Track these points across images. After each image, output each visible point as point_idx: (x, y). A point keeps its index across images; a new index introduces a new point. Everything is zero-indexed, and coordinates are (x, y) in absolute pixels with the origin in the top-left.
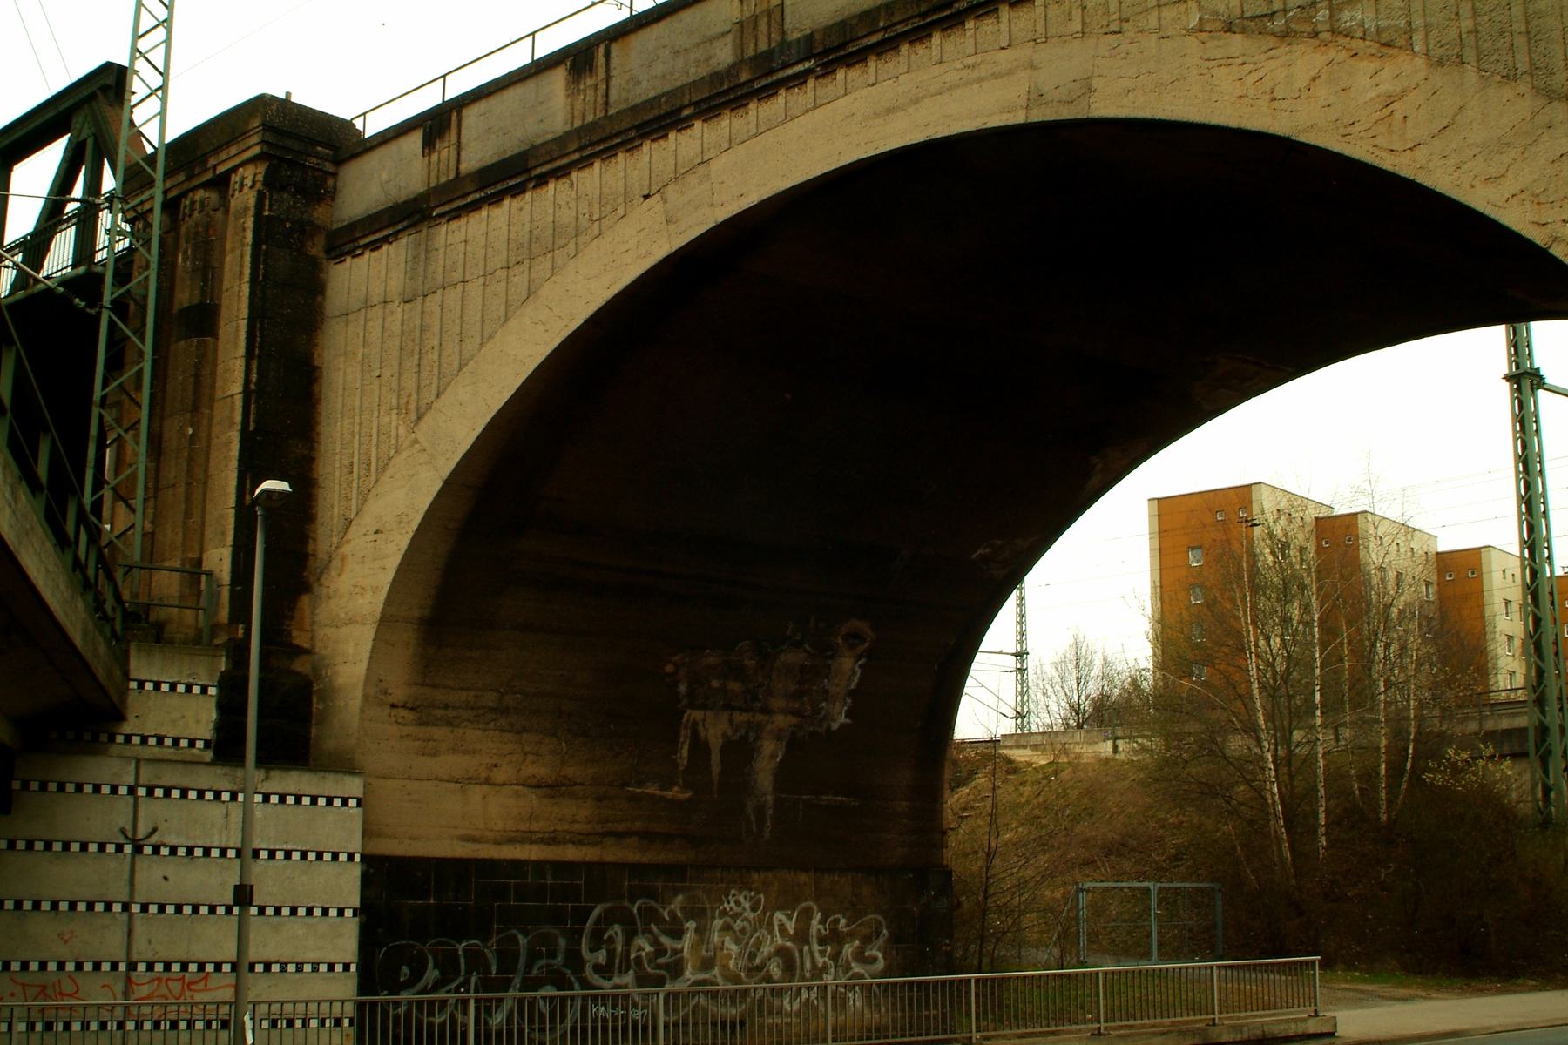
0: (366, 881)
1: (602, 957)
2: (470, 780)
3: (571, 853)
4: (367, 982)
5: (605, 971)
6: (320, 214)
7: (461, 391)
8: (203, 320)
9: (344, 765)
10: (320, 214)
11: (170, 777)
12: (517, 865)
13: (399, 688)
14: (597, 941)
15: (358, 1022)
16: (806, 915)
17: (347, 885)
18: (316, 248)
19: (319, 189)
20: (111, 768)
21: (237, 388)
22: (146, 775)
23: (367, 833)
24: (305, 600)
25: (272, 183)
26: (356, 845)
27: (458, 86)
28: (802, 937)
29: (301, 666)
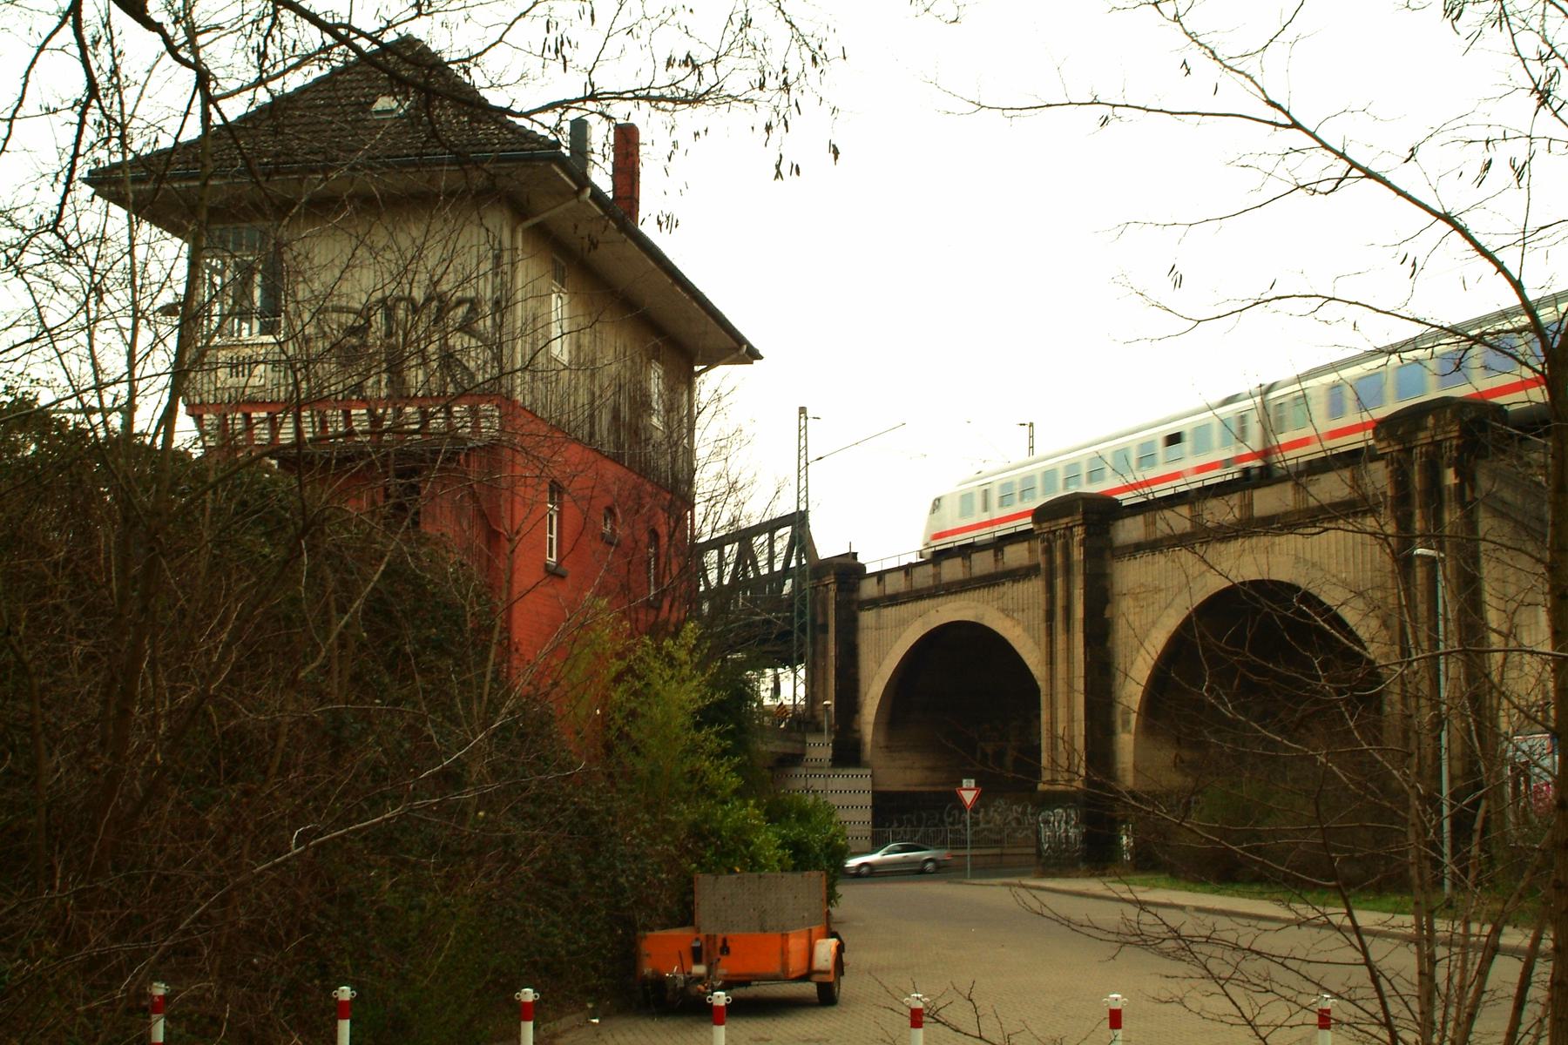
0: (873, 798)
1: (951, 819)
2: (906, 768)
3: (940, 788)
4: (875, 825)
5: (952, 824)
6: (855, 596)
7: (887, 661)
8: (824, 628)
9: (866, 766)
10: (855, 596)
11: (816, 771)
12: (922, 793)
13: (882, 741)
14: (949, 815)
15: (872, 838)
16: (1025, 808)
17: (867, 799)
18: (854, 607)
19: (855, 588)
20: (801, 770)
21: (833, 654)
22: (810, 771)
23: (873, 784)
24: (1109, 606)
25: (839, 590)
26: (870, 788)
27: (886, 567)
28: (1024, 813)
29: (857, 735)
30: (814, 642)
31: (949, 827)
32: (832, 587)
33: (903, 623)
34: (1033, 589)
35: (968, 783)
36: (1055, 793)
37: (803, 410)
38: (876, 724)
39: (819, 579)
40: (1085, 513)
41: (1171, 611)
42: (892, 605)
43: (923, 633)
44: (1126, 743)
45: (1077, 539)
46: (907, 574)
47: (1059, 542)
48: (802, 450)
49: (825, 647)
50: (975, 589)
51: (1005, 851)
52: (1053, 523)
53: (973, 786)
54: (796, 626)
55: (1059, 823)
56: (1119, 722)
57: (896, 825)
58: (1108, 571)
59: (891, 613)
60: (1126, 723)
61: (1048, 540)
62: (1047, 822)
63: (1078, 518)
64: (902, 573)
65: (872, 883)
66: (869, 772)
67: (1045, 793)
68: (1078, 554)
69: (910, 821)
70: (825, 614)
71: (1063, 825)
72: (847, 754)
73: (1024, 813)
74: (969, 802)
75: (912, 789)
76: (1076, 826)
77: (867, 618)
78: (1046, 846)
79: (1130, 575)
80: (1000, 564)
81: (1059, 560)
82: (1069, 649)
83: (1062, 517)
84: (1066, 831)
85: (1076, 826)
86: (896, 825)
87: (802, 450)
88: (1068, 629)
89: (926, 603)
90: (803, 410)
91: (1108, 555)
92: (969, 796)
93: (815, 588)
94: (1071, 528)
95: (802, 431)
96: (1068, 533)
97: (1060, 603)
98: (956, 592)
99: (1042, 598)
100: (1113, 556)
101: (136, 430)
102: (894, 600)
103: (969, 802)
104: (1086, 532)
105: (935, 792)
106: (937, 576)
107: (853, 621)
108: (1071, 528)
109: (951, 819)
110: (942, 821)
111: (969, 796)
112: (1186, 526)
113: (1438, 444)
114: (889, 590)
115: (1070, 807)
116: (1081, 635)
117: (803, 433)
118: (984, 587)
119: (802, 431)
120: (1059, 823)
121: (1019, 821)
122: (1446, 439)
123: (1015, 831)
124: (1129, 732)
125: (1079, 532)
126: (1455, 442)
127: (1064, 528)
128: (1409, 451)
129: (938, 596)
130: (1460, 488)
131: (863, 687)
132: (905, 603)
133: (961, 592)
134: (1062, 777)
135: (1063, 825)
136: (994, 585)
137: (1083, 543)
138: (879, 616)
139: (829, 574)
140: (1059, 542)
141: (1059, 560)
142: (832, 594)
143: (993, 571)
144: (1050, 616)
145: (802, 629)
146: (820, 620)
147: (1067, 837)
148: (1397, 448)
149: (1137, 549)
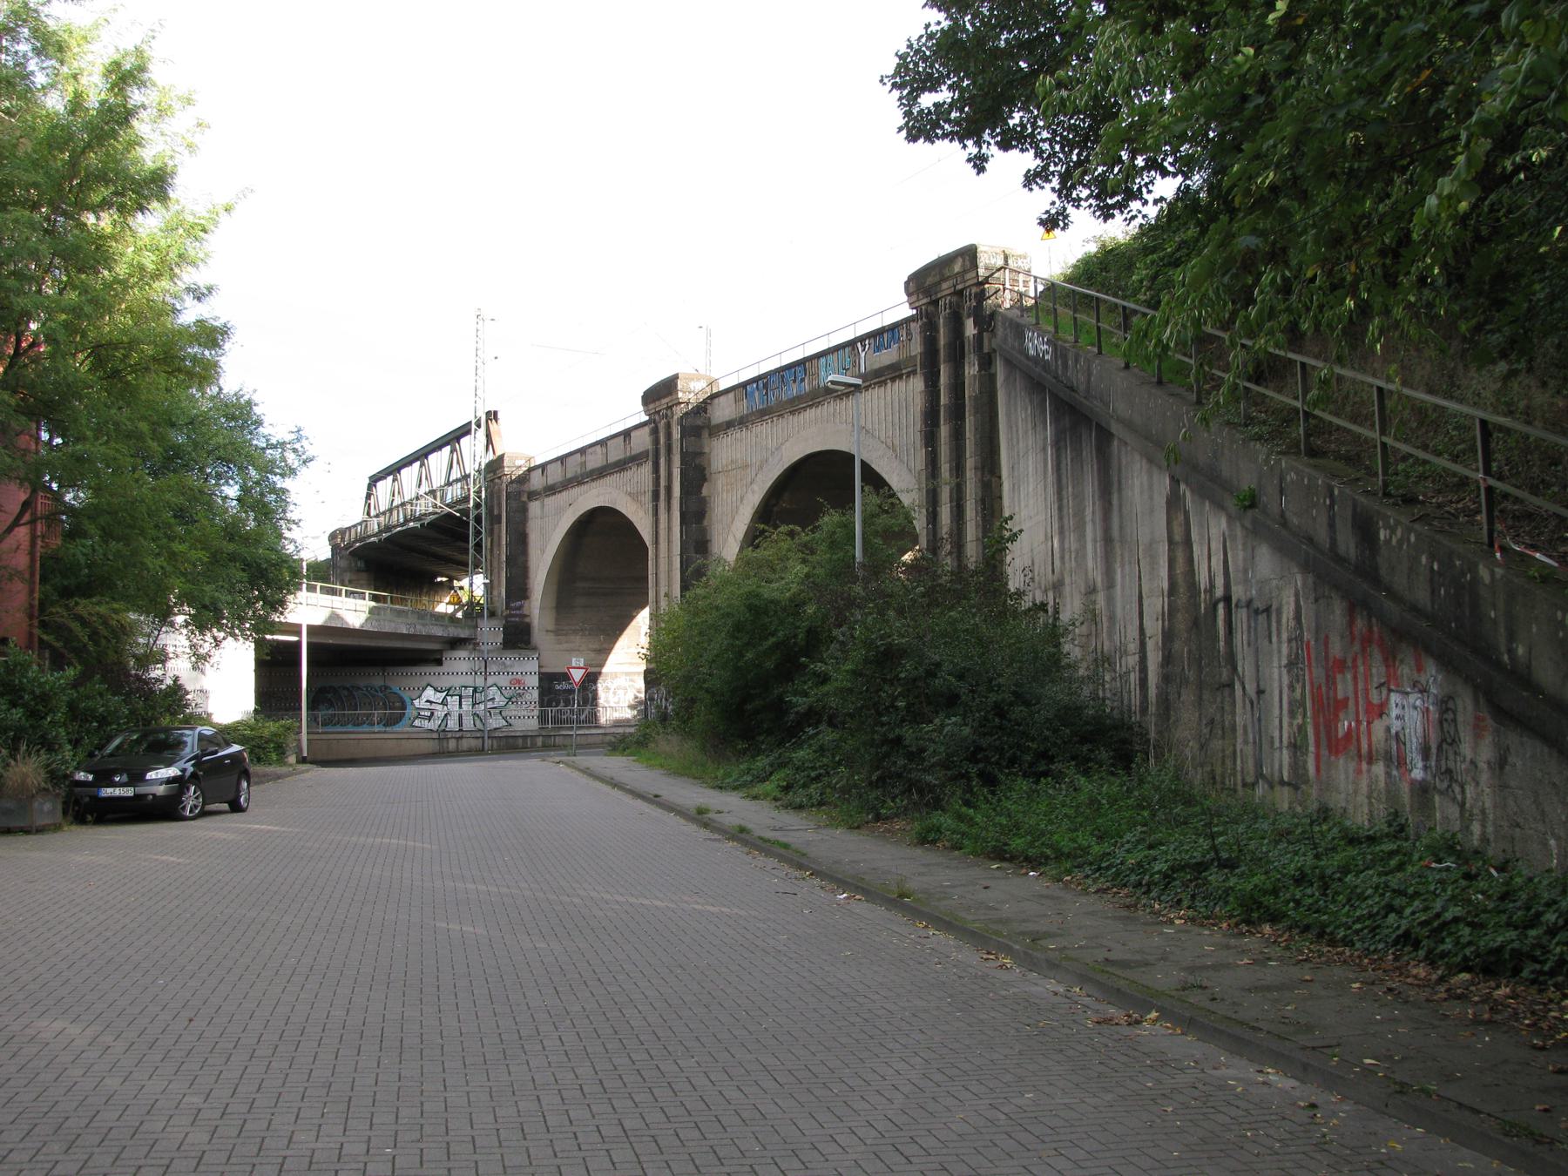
0: (540, 680)
4: (541, 705)
13: (551, 626)
18: (524, 498)
30: (491, 533)
33: (560, 511)
34: (644, 473)
41: (755, 487)
50: (610, 474)
58: (706, 450)
59: (551, 501)
65: (460, 762)
74: (577, 680)
77: (534, 508)
88: (669, 509)
89: (575, 491)
91: (705, 434)
97: (663, 483)
100: (710, 435)
101: (647, 418)
102: (551, 490)
103: (577, 680)
106: (584, 464)
113: (960, 293)
122: (965, 288)
128: (935, 303)
130: (979, 338)
136: (623, 470)
138: (543, 506)
144: (656, 496)
145: (478, 519)
146: (496, 512)
148: (925, 301)
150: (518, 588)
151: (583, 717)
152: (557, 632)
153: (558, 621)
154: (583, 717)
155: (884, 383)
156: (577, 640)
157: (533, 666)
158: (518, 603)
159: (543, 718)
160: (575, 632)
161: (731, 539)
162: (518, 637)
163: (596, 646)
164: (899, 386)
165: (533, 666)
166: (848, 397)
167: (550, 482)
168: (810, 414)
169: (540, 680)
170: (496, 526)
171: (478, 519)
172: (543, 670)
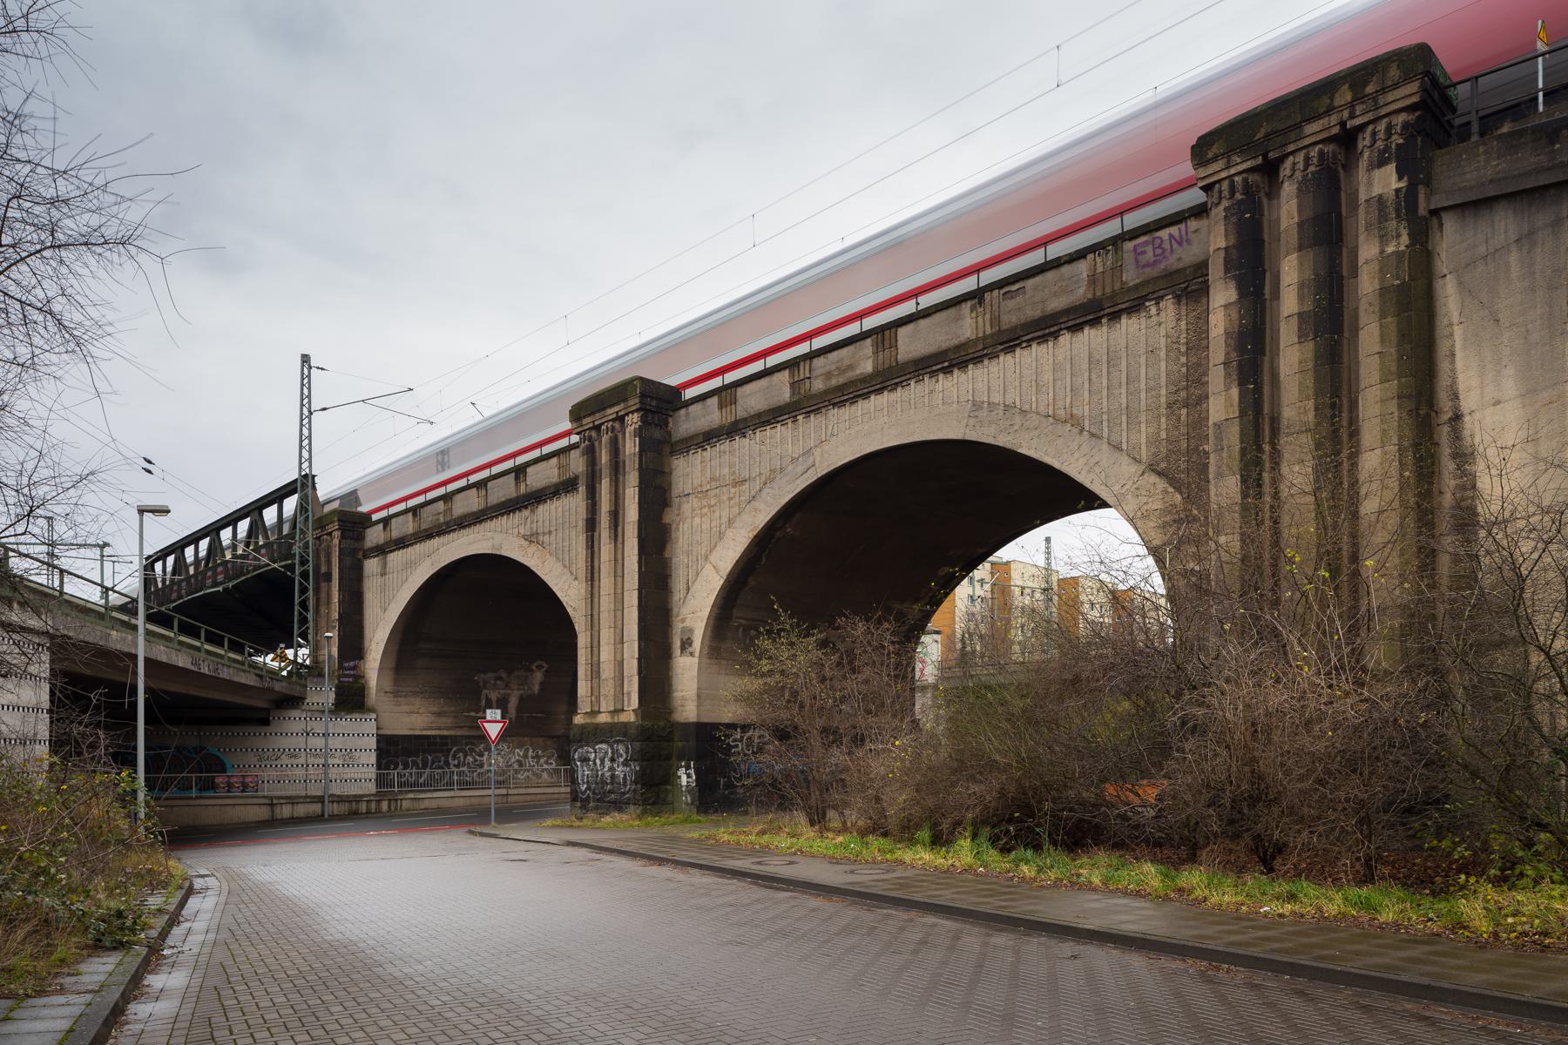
0: (378, 742)
1: (456, 762)
3: (445, 733)
7: (393, 605)
8: (328, 577)
13: (388, 686)
14: (454, 757)
17: (372, 743)
18: (360, 555)
19: (361, 538)
20: (295, 713)
21: (337, 600)
24: (667, 510)
25: (343, 537)
26: (375, 732)
28: (525, 756)
30: (317, 591)
31: (455, 770)
32: (337, 534)
33: (410, 565)
35: (493, 714)
36: (597, 727)
37: (305, 359)
38: (380, 669)
39: (323, 527)
40: (643, 396)
42: (398, 549)
43: (432, 572)
44: (687, 672)
45: (630, 430)
46: (415, 515)
47: (605, 439)
48: (305, 398)
49: (329, 597)
50: (491, 519)
51: (510, 792)
52: (598, 415)
53: (499, 718)
54: (297, 572)
55: (602, 761)
56: (677, 644)
57: (401, 767)
59: (395, 558)
60: (686, 644)
61: (590, 438)
62: (585, 760)
63: (634, 402)
64: (410, 515)
66: (374, 716)
67: (583, 727)
68: (631, 447)
69: (415, 764)
70: (329, 562)
71: (607, 763)
72: (351, 699)
73: (525, 756)
75: (418, 733)
76: (625, 764)
77: (371, 565)
78: (584, 787)
79: (689, 472)
80: (523, 486)
81: (604, 457)
82: (619, 562)
83: (611, 406)
84: (612, 769)
85: (625, 764)
86: (401, 767)
87: (305, 398)
89: (436, 542)
90: (305, 359)
91: (667, 449)
92: (493, 730)
93: (318, 538)
94: (623, 417)
95: (305, 381)
96: (617, 425)
98: (469, 526)
99: (582, 513)
104: (643, 420)
105: (440, 736)
107: (359, 569)
108: (623, 417)
109: (456, 762)
110: (447, 764)
111: (493, 730)
112: (786, 395)
114: (395, 534)
115: (618, 742)
116: (636, 541)
117: (306, 381)
118: (502, 515)
119: (305, 381)
120: (602, 761)
121: (521, 765)
123: (516, 772)
124: (692, 654)
125: (634, 420)
126: (1401, 119)
127: (613, 420)
129: (449, 532)
131: (368, 633)
132: (411, 545)
133: (475, 524)
134: (606, 705)
135: (607, 763)
137: (639, 433)
139: (332, 522)
140: (605, 439)
141: (604, 457)
142: (336, 541)
143: (514, 495)
145: (305, 575)
146: (323, 569)
147: (613, 776)
149: (710, 437)
150: (353, 645)
151: (421, 781)
152: (396, 694)
153: (396, 682)
154: (421, 781)
155: (1055, 336)
156: (418, 702)
157: (369, 726)
158: (352, 664)
159: (381, 781)
160: (415, 694)
161: (708, 571)
162: (351, 699)
163: (435, 709)
164: (1130, 328)
165: (369, 726)
166: (514, 513)
167: (424, 526)
168: (875, 401)
169: (378, 742)
170: (324, 585)
171: (305, 575)
172: (381, 732)
